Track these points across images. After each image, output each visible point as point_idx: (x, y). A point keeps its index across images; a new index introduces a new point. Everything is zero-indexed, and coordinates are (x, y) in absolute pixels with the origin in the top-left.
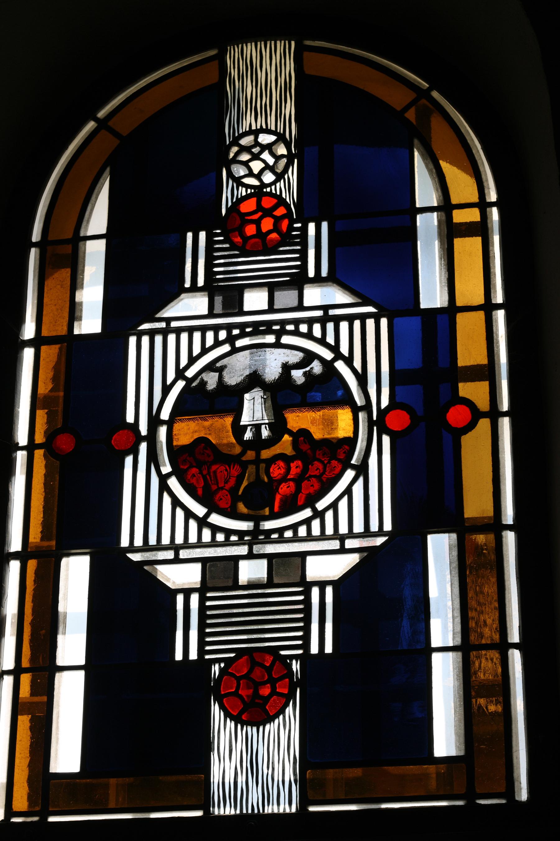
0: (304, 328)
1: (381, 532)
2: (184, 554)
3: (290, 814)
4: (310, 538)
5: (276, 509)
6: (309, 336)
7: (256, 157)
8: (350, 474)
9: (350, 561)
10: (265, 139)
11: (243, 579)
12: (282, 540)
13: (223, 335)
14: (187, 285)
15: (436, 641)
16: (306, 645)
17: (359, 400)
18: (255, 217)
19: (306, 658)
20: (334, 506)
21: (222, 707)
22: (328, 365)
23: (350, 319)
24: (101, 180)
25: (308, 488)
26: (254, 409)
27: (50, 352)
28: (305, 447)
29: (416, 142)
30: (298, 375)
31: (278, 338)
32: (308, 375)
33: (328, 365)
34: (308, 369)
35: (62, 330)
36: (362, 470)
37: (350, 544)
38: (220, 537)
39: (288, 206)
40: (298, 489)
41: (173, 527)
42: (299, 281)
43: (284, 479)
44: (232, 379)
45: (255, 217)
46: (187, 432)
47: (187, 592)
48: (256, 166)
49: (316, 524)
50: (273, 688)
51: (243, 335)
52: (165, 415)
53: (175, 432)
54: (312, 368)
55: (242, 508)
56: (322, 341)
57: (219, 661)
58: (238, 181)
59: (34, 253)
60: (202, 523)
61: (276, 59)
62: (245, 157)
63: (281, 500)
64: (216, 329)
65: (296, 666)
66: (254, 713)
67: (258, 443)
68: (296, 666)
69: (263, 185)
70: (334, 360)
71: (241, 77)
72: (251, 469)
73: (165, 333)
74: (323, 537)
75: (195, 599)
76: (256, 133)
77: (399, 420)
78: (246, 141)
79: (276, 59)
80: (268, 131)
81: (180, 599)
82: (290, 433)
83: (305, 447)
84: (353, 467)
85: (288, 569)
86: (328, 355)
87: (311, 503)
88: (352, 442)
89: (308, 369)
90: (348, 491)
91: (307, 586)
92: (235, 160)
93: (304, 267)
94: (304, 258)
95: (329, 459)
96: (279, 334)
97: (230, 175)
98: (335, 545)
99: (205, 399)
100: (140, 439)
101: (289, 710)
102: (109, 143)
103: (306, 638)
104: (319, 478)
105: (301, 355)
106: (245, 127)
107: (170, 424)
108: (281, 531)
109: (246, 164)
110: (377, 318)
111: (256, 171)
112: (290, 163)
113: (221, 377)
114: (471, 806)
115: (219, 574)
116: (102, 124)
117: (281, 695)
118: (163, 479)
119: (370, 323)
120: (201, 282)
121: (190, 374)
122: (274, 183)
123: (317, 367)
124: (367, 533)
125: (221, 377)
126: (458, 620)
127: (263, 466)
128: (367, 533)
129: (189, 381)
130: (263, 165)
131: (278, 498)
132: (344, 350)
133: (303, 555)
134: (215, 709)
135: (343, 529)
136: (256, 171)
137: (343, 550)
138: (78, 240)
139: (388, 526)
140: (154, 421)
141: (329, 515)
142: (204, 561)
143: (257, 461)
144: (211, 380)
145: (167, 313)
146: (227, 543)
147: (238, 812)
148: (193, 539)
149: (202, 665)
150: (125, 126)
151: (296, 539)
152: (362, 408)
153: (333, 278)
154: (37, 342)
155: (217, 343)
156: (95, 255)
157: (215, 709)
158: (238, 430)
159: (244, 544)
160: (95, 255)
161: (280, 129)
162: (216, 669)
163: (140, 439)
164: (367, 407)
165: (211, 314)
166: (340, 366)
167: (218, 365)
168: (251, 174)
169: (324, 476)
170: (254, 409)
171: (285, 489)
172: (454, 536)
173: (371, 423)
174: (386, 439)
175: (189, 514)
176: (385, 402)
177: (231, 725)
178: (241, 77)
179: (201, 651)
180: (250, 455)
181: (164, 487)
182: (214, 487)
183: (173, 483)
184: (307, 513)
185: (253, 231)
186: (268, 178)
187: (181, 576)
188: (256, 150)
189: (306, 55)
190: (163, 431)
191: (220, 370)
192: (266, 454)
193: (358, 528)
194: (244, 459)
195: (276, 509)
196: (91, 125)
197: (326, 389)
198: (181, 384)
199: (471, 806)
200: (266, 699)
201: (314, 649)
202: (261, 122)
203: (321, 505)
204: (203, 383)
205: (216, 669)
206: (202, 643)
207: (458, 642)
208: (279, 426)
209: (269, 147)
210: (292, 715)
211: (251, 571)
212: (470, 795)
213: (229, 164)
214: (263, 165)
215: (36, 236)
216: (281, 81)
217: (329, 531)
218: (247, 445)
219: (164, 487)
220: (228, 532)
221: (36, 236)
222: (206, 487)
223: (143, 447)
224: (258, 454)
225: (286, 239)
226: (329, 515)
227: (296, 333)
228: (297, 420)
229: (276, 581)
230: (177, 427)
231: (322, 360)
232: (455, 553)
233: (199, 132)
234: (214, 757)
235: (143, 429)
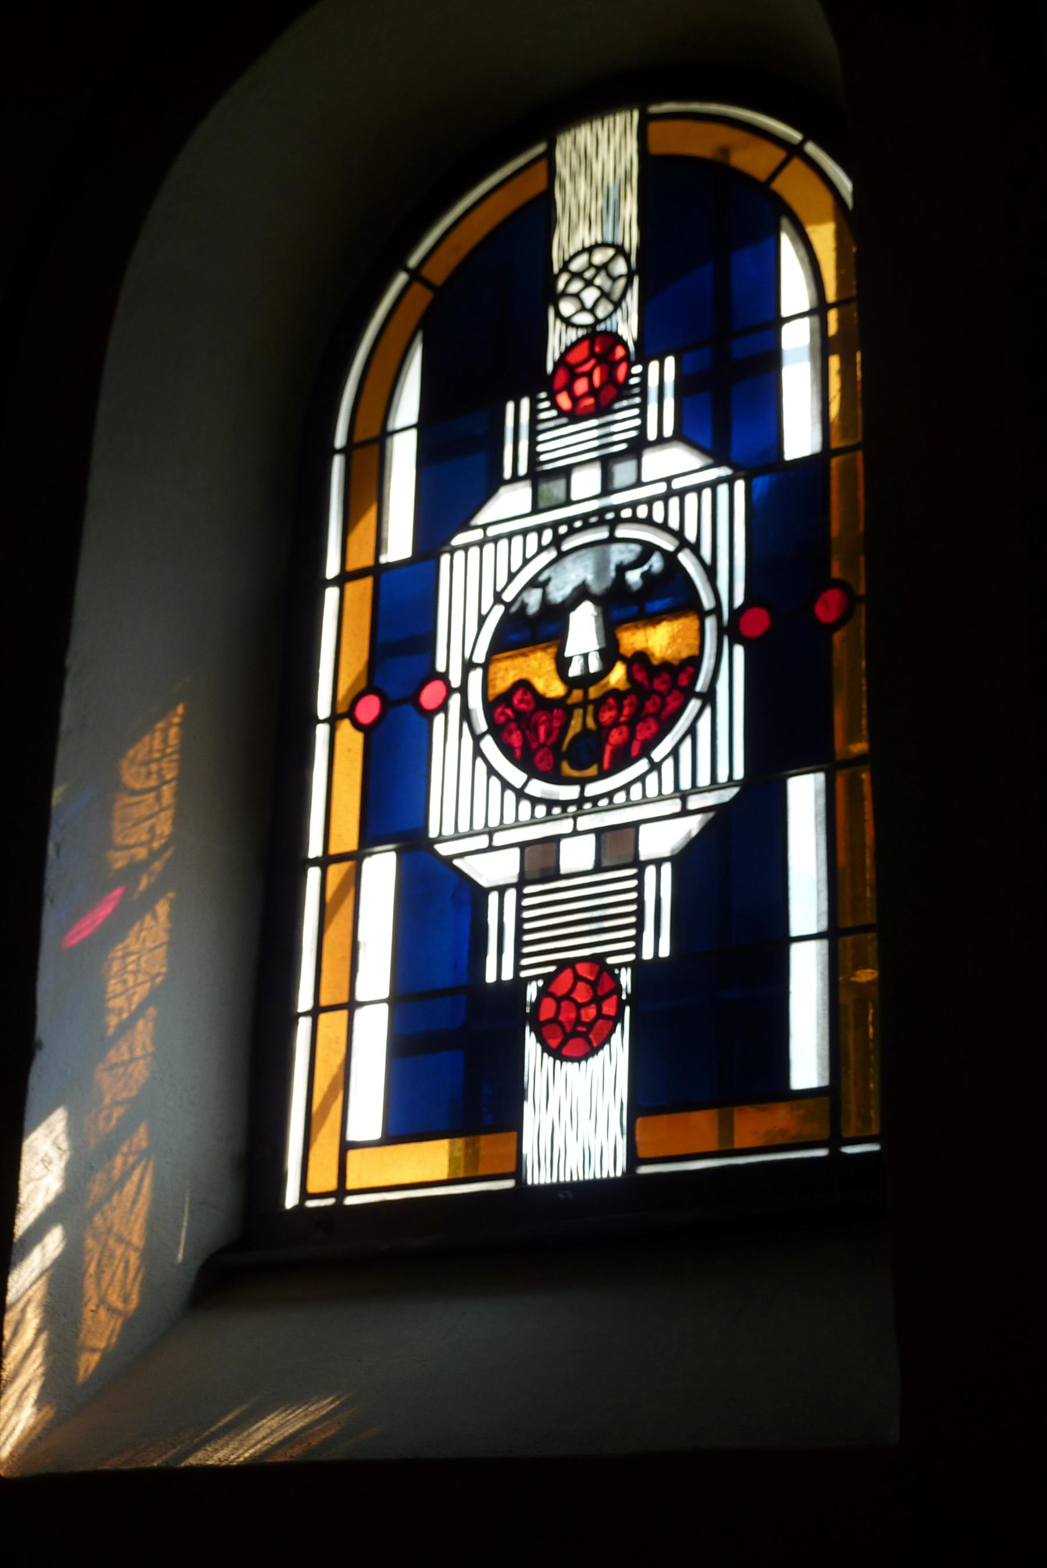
0: (642, 512)
1: (731, 782)
2: (499, 839)
3: (616, 1179)
4: (645, 800)
5: (606, 764)
6: (649, 521)
7: (589, 283)
8: (694, 705)
9: (693, 825)
10: (600, 257)
11: (566, 865)
12: (612, 807)
13: (548, 536)
14: (507, 474)
15: (796, 928)
16: (637, 950)
17: (708, 603)
18: (586, 367)
19: (638, 967)
20: (675, 753)
21: (540, 1039)
22: (670, 558)
23: (698, 489)
24: (412, 351)
25: (643, 733)
26: (583, 631)
27: (361, 590)
28: (640, 676)
29: (785, 222)
30: (634, 577)
31: (612, 532)
32: (645, 576)
33: (670, 558)
34: (646, 568)
35: (367, 561)
36: (709, 698)
37: (477, 535)
38: (541, 811)
39: (625, 345)
40: (632, 736)
41: (492, 804)
42: (638, 446)
43: (615, 723)
44: (559, 593)
45: (586, 367)
46: (508, 673)
47: (502, 890)
48: (590, 296)
49: (652, 779)
50: (599, 1009)
51: (572, 531)
52: (480, 657)
53: (491, 676)
54: (651, 567)
55: (566, 769)
56: (664, 527)
57: (536, 978)
58: (568, 322)
59: (338, 464)
60: (520, 794)
61: (616, 139)
62: (576, 286)
63: (612, 753)
64: (539, 529)
65: (626, 978)
66: (574, 1042)
67: (587, 680)
68: (626, 978)
69: (598, 321)
70: (678, 550)
71: (573, 176)
72: (578, 713)
73: (481, 544)
74: (661, 798)
75: (511, 895)
76: (590, 250)
77: (758, 623)
78: (576, 265)
79: (616, 139)
80: (604, 245)
81: (493, 898)
82: (623, 659)
83: (640, 676)
84: (699, 695)
85: (617, 847)
86: (668, 544)
87: (646, 751)
88: (694, 662)
89: (646, 568)
90: (692, 731)
91: (641, 866)
92: (564, 294)
93: (642, 429)
94: (643, 415)
95: (660, 695)
96: (613, 525)
97: (558, 314)
98: (483, 842)
99: (530, 627)
100: (450, 691)
101: (616, 1038)
102: (422, 297)
103: (638, 938)
104: (656, 716)
105: (637, 548)
106: (577, 246)
107: (485, 666)
108: (610, 795)
109: (577, 296)
110: (730, 481)
111: (589, 304)
112: (629, 284)
113: (545, 595)
114: (836, 1155)
115: (540, 863)
116: (415, 275)
117: (607, 1017)
118: (477, 738)
119: (723, 490)
120: (523, 470)
121: (508, 597)
122: (610, 316)
123: (656, 563)
124: (714, 785)
125: (545, 595)
126: (824, 895)
127: (591, 709)
128: (714, 785)
129: (509, 606)
130: (593, 297)
131: (608, 749)
132: (690, 535)
133: (635, 825)
134: (531, 1041)
135: (685, 784)
136: (589, 304)
137: (685, 812)
138: (383, 436)
139: (739, 774)
140: (468, 666)
141: (668, 766)
142: (523, 846)
143: (584, 703)
144: (533, 600)
145: (481, 519)
146: (549, 818)
147: (555, 1180)
148: (509, 820)
149: (519, 984)
150: (437, 273)
151: (629, 804)
152: (710, 613)
153: (680, 436)
154: (343, 579)
155: (541, 549)
156: (403, 453)
157: (531, 1041)
158: (562, 664)
159: (567, 817)
160: (403, 453)
161: (619, 241)
162: (532, 992)
163: (450, 691)
164: (717, 610)
165: (536, 510)
166: (685, 559)
167: (543, 578)
168: (583, 309)
169: (664, 713)
170: (583, 631)
171: (616, 737)
172: (821, 777)
173: (721, 631)
174: (739, 651)
175: (506, 785)
176: (739, 600)
177: (548, 1060)
178: (573, 176)
179: (518, 968)
180: (577, 695)
181: (478, 752)
182: (534, 745)
183: (489, 745)
184: (642, 765)
185: (601, 378)
186: (601, 312)
187: (494, 869)
188: (588, 275)
189: (653, 127)
190: (476, 677)
191: (544, 585)
192: (594, 692)
193: (704, 780)
194: (570, 701)
195: (606, 764)
196: (402, 279)
197: (667, 592)
198: (500, 610)
199: (836, 1155)
200: (590, 1025)
201: (647, 954)
202: (596, 236)
203: (657, 754)
204: (524, 606)
205: (532, 992)
206: (640, 889)
207: (824, 925)
208: (610, 653)
209: (605, 267)
210: (619, 1047)
211: (577, 854)
212: (834, 1142)
213: (555, 298)
214: (593, 297)
215: (340, 440)
216: (621, 171)
217: (668, 788)
218: (571, 684)
219: (478, 752)
220: (550, 803)
221: (340, 440)
222: (525, 746)
223: (455, 701)
224: (586, 694)
225: (623, 391)
226: (668, 766)
227: (634, 520)
228: (632, 640)
229: (605, 863)
230: (493, 668)
231: (664, 553)
232: (822, 801)
233: (518, 262)
234: (528, 1107)
235: (455, 681)
